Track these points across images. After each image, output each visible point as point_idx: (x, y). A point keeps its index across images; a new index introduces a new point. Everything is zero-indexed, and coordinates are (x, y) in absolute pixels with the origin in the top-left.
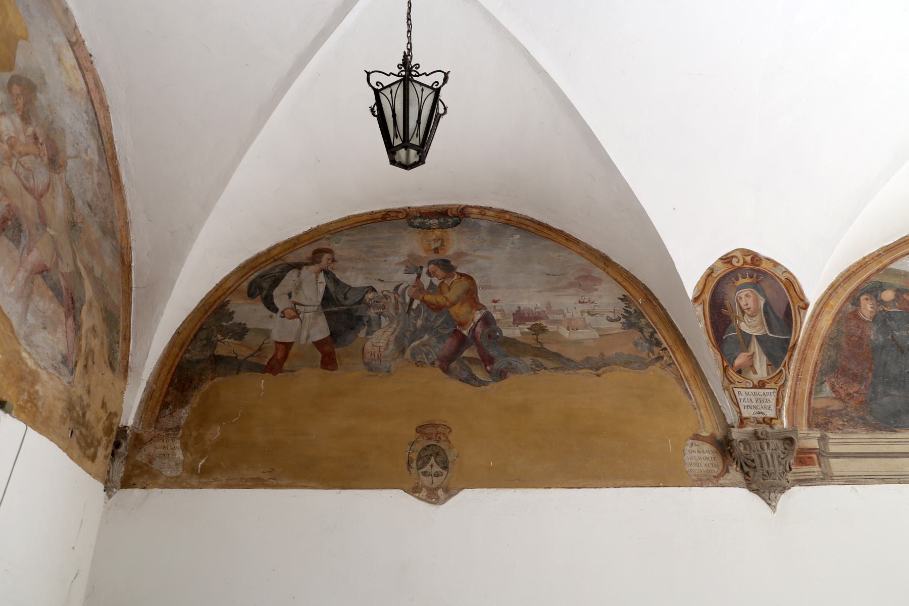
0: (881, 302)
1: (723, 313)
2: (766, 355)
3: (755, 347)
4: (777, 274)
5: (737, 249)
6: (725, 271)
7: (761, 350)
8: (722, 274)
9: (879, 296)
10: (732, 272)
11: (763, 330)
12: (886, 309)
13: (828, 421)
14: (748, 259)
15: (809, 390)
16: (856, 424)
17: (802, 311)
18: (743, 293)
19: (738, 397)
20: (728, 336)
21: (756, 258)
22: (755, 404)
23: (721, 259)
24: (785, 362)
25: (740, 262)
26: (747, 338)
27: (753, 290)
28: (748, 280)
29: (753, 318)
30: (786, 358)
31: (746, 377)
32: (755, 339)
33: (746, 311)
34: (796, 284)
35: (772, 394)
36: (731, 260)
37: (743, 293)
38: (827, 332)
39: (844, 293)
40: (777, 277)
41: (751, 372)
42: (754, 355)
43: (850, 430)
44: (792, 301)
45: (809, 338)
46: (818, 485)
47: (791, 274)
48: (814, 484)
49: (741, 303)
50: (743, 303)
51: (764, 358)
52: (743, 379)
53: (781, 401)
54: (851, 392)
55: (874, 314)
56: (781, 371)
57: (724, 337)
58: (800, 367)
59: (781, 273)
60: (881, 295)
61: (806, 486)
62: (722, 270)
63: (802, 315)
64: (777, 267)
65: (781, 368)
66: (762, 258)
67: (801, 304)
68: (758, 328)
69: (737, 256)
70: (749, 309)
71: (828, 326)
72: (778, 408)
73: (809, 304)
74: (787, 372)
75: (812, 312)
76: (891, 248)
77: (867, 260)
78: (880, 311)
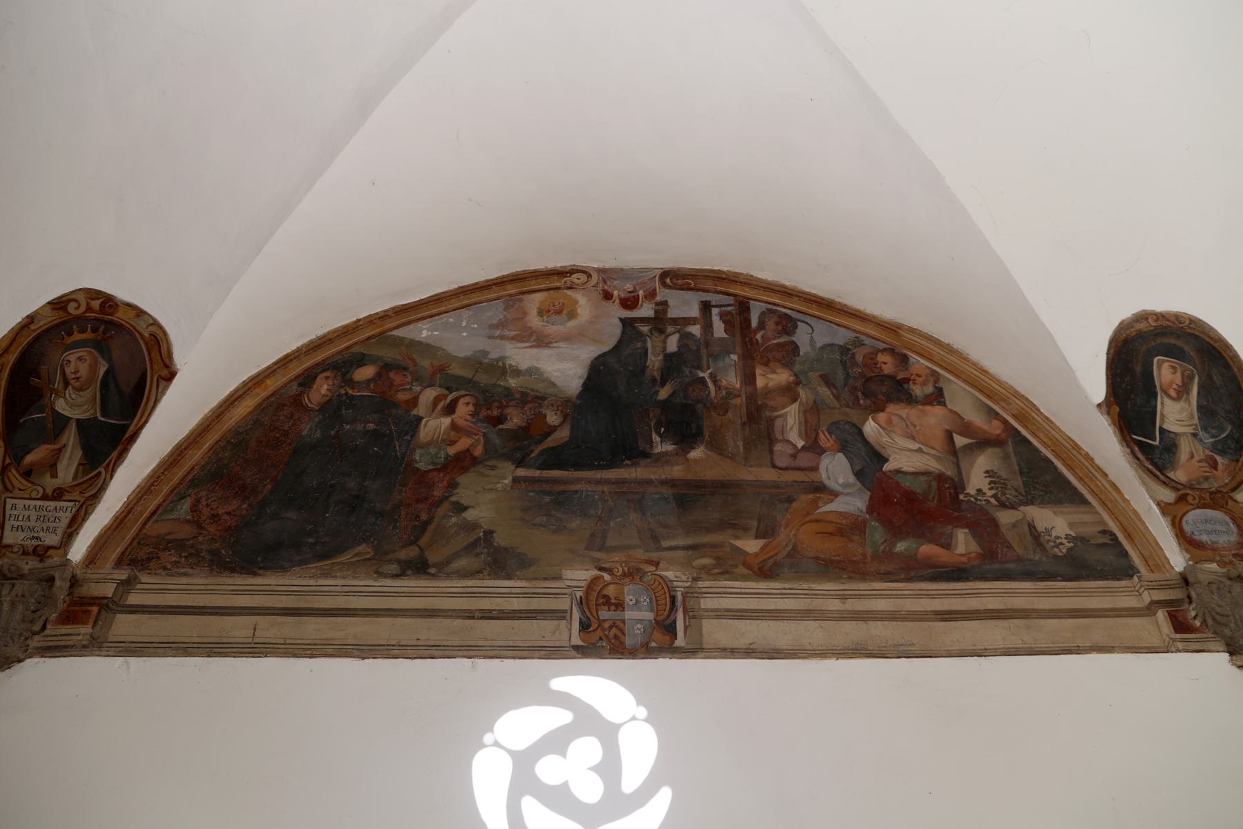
0: (351, 383)
1: (31, 383)
2: (83, 449)
3: (70, 437)
4: (138, 328)
5: (80, 290)
6: (52, 321)
7: (78, 441)
8: (47, 326)
9: (350, 373)
10: (64, 322)
11: (92, 411)
12: (350, 392)
13: (154, 555)
14: (96, 304)
15: (154, 508)
16: (199, 561)
17: (162, 383)
18: (74, 354)
19: (8, 512)
20: (30, 419)
21: (108, 302)
22: (32, 524)
23: (50, 303)
24: (110, 461)
25: (81, 309)
26: (61, 422)
27: (93, 351)
28: (88, 335)
29: (81, 393)
30: (114, 455)
31: (34, 481)
32: (74, 424)
33: (72, 382)
34: (165, 342)
35: (69, 509)
36: (67, 306)
37: (73, 356)
38: (236, 424)
39: (297, 369)
40: (139, 332)
41: (48, 475)
42: (64, 450)
43: (183, 570)
44: (152, 368)
45: (205, 431)
46: (72, 656)
47: (161, 328)
48: (65, 654)
49: (66, 369)
50: (69, 370)
51: (79, 454)
52: (30, 485)
53: (80, 520)
54: (220, 511)
55: (328, 398)
56: (100, 473)
57: (21, 421)
58: (163, 473)
59: (145, 326)
60: (353, 373)
61: (50, 657)
62: (50, 318)
63: (160, 389)
64: (140, 318)
65: (101, 469)
66: (119, 304)
67: (165, 373)
68: (86, 407)
69: (78, 299)
70: (77, 378)
71: (245, 414)
72: (69, 531)
73: (176, 373)
74: (108, 476)
75: (229, 394)
76: (409, 308)
77: (361, 323)
78: (340, 396)
